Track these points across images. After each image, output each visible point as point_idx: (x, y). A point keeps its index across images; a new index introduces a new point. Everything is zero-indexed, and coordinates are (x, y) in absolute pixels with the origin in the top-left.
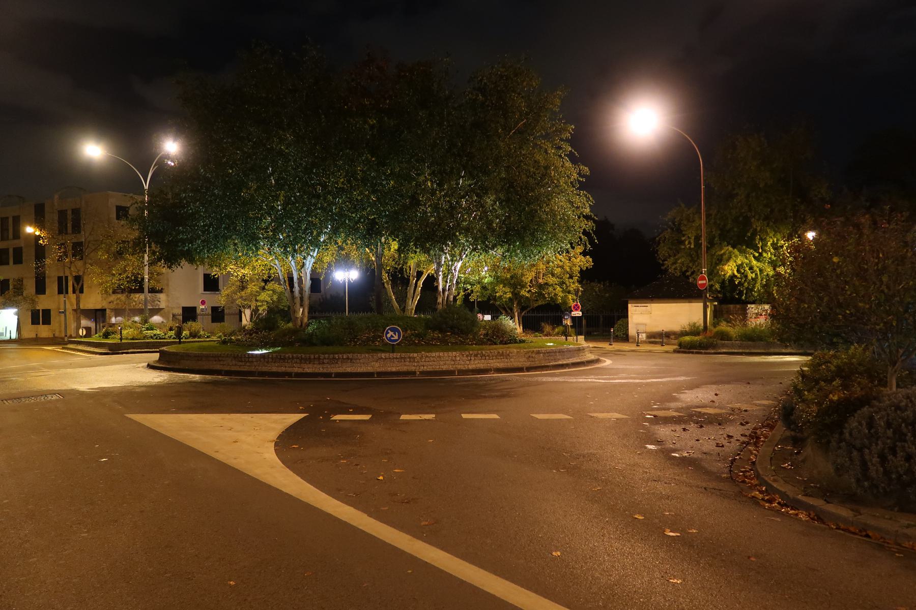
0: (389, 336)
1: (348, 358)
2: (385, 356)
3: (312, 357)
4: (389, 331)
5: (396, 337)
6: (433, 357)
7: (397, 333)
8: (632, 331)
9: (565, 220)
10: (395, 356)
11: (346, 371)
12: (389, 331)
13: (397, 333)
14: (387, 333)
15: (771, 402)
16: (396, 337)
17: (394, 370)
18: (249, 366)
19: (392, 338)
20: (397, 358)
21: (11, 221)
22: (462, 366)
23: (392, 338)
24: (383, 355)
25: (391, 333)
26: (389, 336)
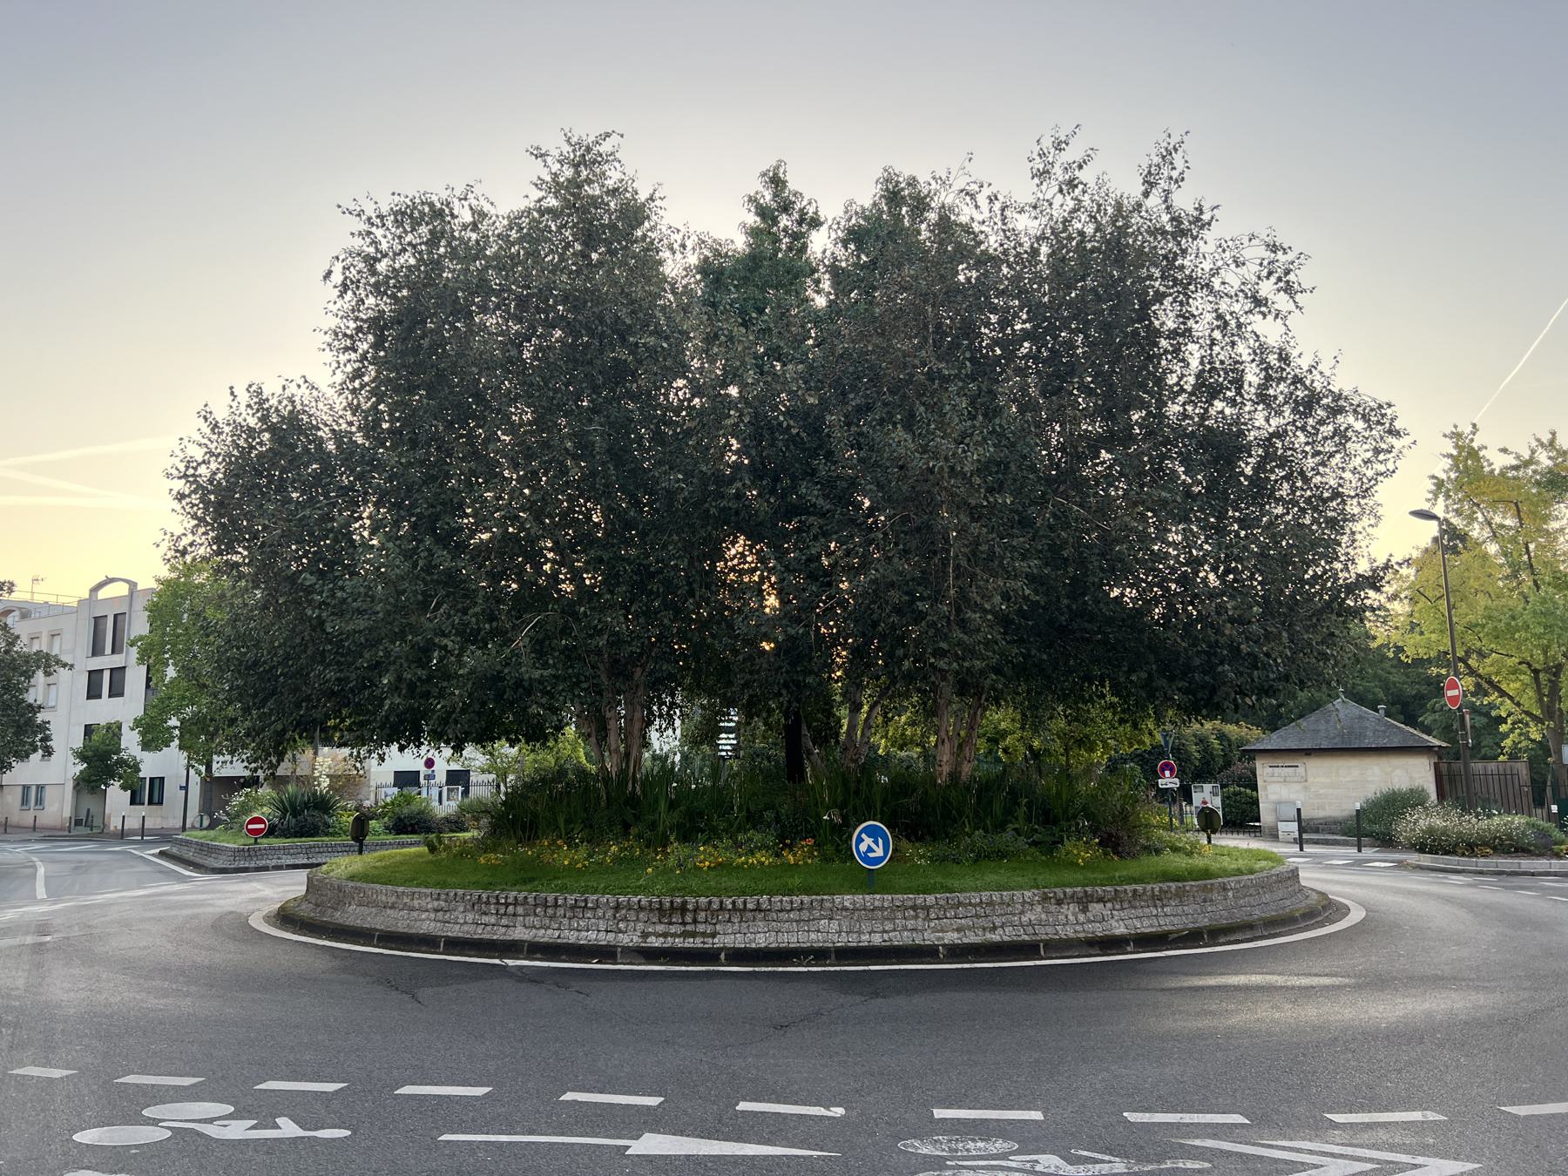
0: (863, 847)
1: (758, 909)
2: (854, 903)
3: (728, 903)
4: (863, 836)
5: (879, 852)
6: (974, 906)
7: (880, 841)
8: (1266, 817)
9: (726, 621)
10: (877, 903)
11: (413, 931)
12: (863, 836)
13: (880, 841)
14: (860, 840)
15: (1170, 1024)
16: (879, 852)
17: (877, 940)
18: (507, 926)
19: (871, 855)
20: (882, 909)
21: (33, 790)
22: (1050, 930)
23: (871, 855)
24: (847, 900)
25: (868, 841)
26: (863, 847)
